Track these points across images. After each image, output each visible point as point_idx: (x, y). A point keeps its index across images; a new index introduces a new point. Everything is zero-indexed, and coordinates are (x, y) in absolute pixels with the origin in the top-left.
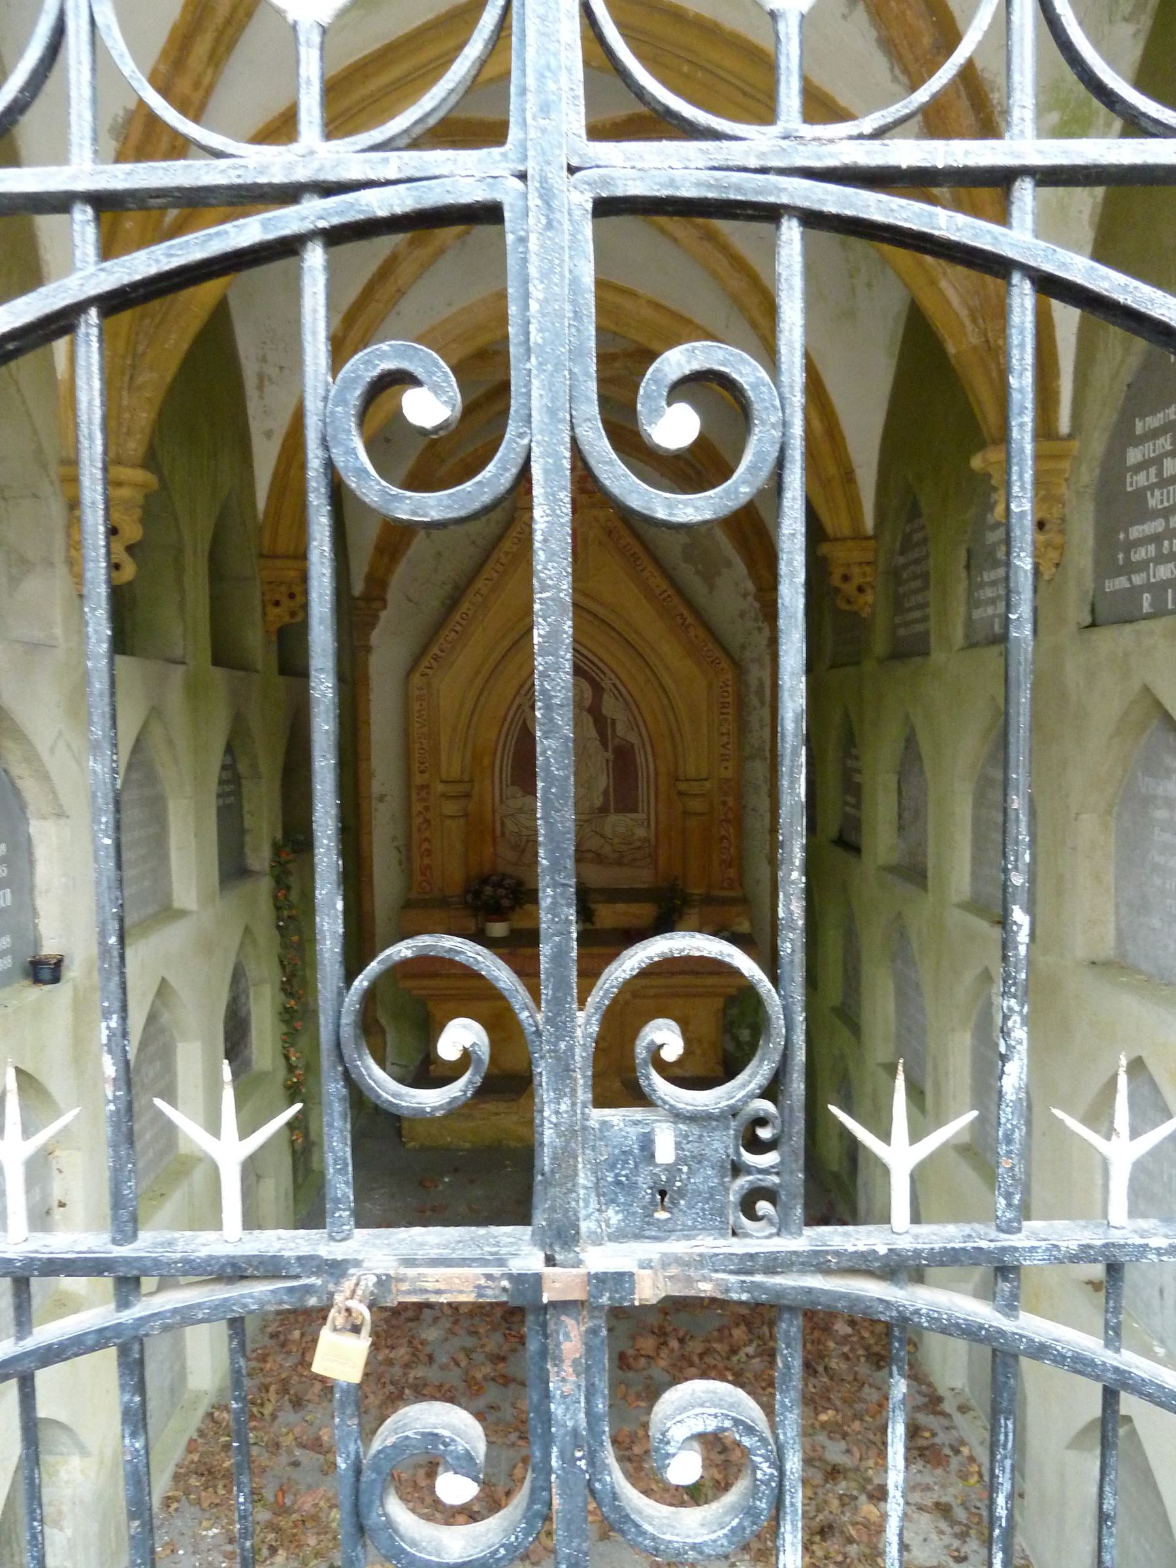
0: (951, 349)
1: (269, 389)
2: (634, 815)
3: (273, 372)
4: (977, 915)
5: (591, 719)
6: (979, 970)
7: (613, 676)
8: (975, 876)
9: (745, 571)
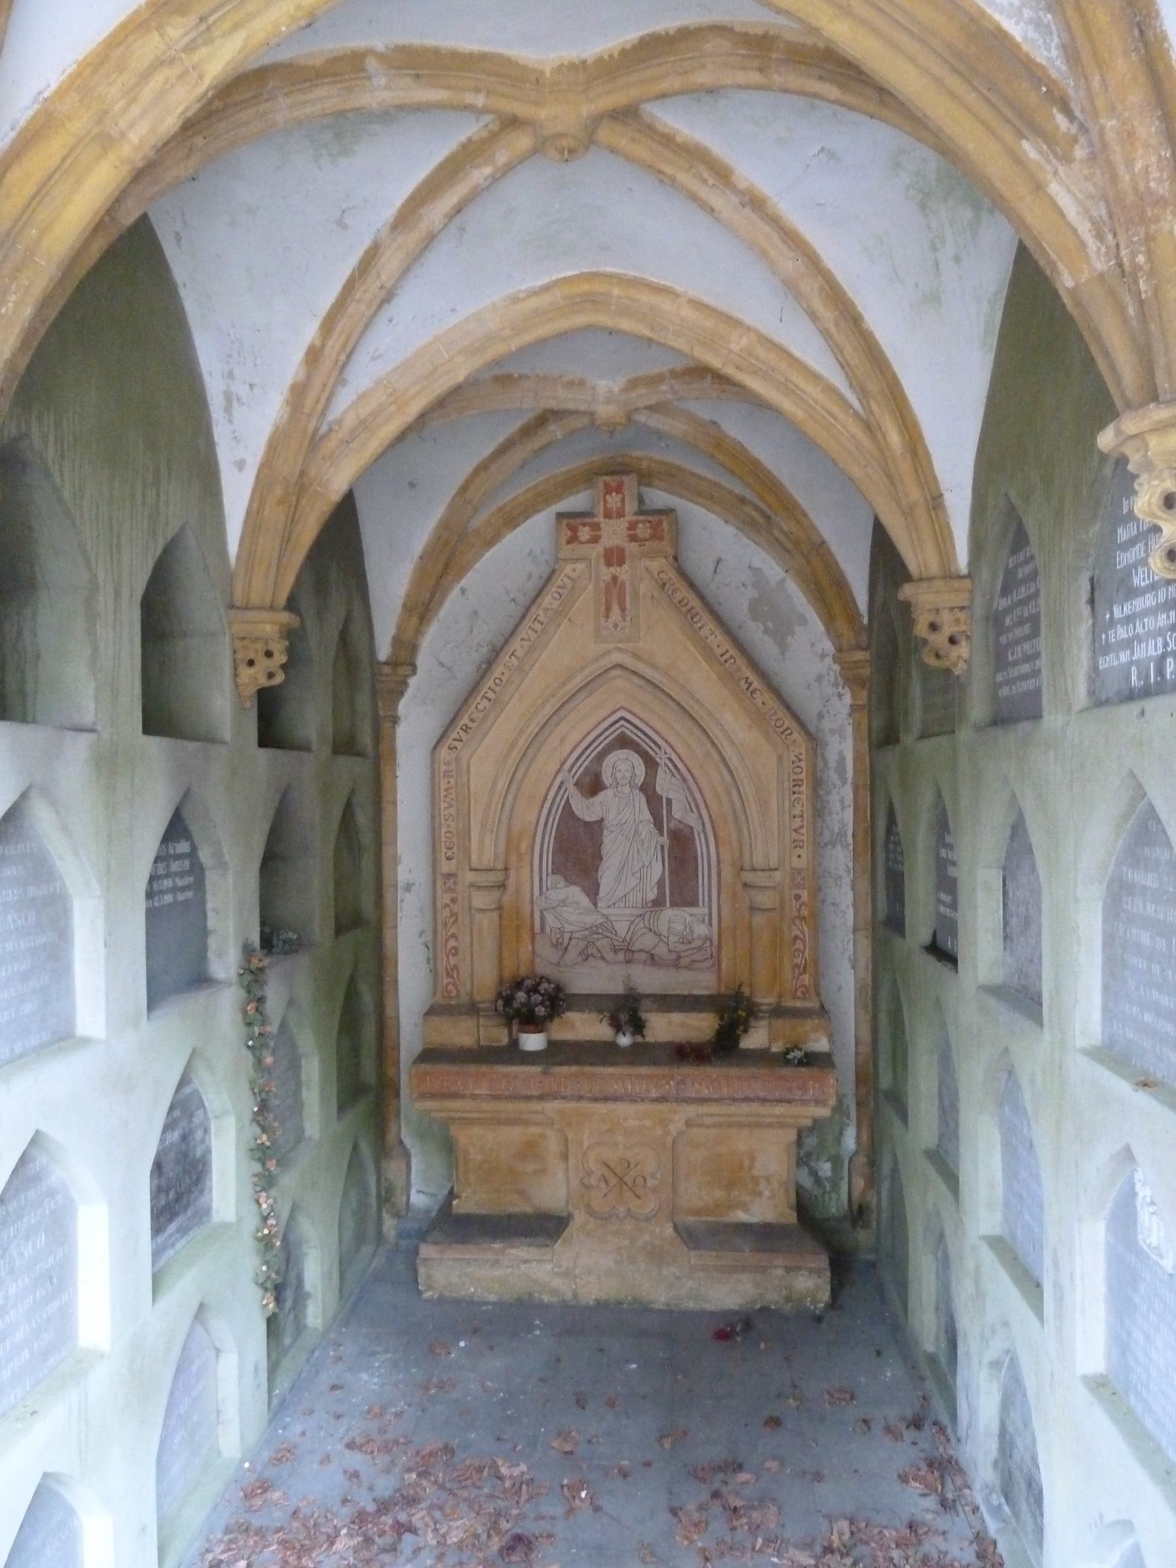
0: (1066, 281)
1: (238, 411)
2: (693, 910)
3: (241, 389)
4: (1112, 1070)
5: (643, 799)
6: (1117, 1147)
7: (669, 750)
8: (1108, 1013)
9: (822, 628)
